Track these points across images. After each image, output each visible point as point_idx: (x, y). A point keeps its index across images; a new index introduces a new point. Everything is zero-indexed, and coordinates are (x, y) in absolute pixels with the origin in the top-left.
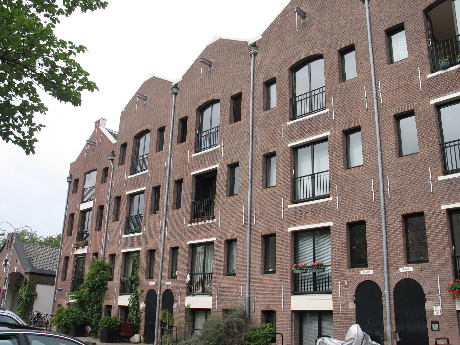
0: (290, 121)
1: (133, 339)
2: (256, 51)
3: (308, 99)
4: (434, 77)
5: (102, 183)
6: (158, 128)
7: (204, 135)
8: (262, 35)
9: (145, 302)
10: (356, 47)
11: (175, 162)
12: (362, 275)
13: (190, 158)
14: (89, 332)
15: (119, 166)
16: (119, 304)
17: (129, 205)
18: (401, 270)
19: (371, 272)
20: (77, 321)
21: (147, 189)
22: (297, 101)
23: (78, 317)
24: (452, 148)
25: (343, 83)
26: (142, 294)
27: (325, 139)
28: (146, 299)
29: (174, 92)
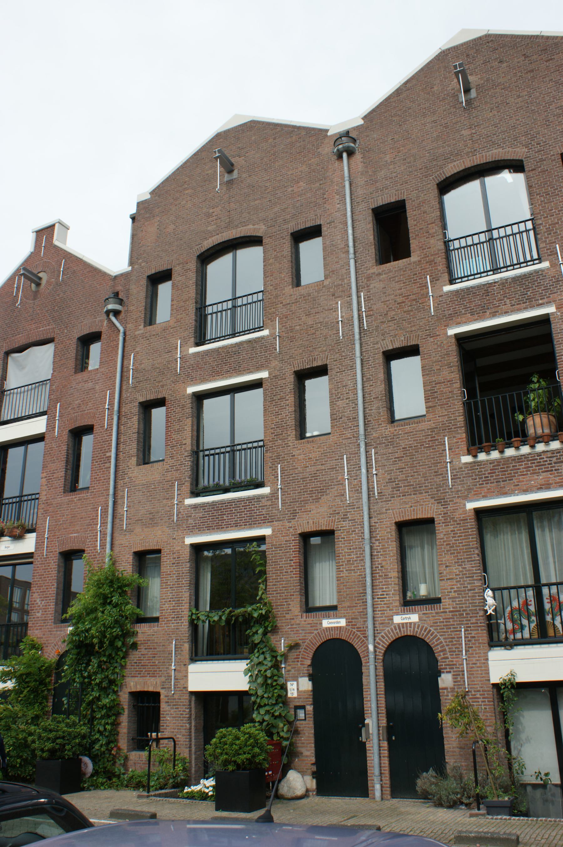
0: (195, 347)
1: (290, 788)
2: (352, 145)
3: (229, 311)
4: (198, 353)
5: (76, 372)
6: (291, 231)
7: (239, 304)
8: (150, 193)
9: (312, 678)
10: (324, 229)
11: (375, 307)
12: (399, 624)
13: (435, 296)
14: (89, 775)
15: (145, 326)
16: (192, 687)
17: (195, 420)
18: (397, 619)
19: (342, 622)
20: (64, 745)
21: (272, 377)
22: (230, 309)
23: (70, 734)
24: (212, 457)
25: (151, 327)
26: (292, 655)
27: (257, 384)
28: (311, 669)
29: (348, 147)
